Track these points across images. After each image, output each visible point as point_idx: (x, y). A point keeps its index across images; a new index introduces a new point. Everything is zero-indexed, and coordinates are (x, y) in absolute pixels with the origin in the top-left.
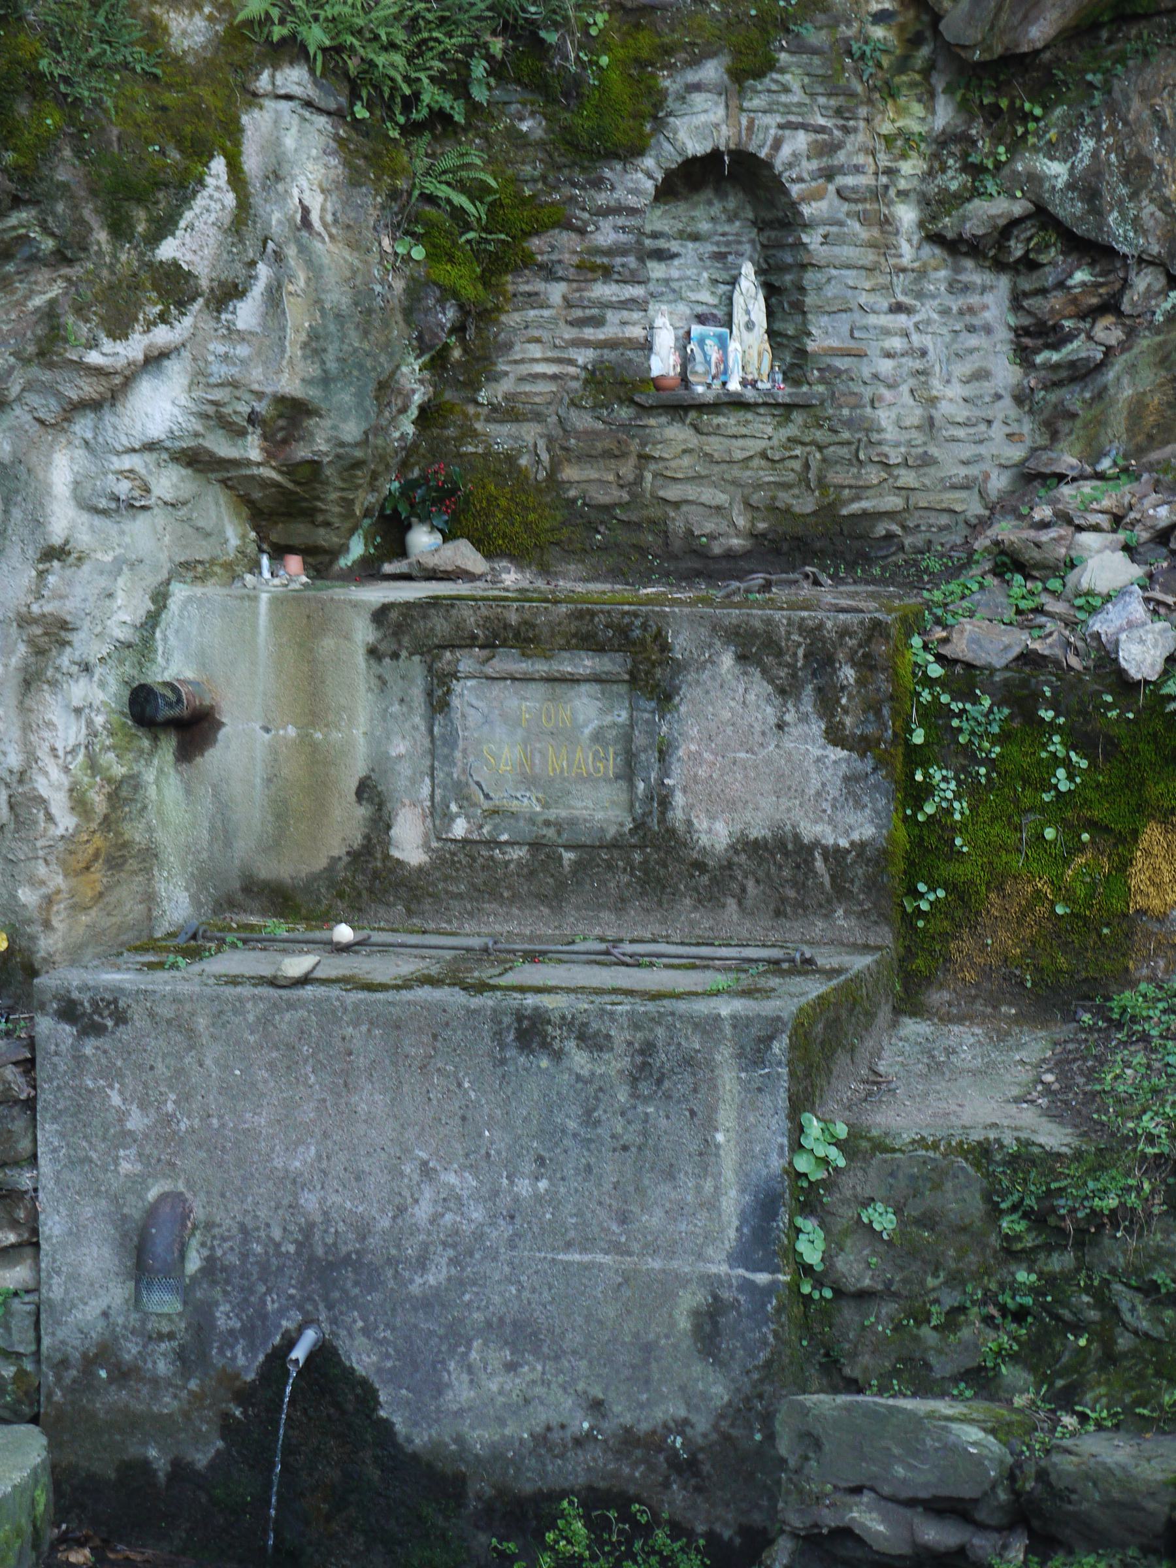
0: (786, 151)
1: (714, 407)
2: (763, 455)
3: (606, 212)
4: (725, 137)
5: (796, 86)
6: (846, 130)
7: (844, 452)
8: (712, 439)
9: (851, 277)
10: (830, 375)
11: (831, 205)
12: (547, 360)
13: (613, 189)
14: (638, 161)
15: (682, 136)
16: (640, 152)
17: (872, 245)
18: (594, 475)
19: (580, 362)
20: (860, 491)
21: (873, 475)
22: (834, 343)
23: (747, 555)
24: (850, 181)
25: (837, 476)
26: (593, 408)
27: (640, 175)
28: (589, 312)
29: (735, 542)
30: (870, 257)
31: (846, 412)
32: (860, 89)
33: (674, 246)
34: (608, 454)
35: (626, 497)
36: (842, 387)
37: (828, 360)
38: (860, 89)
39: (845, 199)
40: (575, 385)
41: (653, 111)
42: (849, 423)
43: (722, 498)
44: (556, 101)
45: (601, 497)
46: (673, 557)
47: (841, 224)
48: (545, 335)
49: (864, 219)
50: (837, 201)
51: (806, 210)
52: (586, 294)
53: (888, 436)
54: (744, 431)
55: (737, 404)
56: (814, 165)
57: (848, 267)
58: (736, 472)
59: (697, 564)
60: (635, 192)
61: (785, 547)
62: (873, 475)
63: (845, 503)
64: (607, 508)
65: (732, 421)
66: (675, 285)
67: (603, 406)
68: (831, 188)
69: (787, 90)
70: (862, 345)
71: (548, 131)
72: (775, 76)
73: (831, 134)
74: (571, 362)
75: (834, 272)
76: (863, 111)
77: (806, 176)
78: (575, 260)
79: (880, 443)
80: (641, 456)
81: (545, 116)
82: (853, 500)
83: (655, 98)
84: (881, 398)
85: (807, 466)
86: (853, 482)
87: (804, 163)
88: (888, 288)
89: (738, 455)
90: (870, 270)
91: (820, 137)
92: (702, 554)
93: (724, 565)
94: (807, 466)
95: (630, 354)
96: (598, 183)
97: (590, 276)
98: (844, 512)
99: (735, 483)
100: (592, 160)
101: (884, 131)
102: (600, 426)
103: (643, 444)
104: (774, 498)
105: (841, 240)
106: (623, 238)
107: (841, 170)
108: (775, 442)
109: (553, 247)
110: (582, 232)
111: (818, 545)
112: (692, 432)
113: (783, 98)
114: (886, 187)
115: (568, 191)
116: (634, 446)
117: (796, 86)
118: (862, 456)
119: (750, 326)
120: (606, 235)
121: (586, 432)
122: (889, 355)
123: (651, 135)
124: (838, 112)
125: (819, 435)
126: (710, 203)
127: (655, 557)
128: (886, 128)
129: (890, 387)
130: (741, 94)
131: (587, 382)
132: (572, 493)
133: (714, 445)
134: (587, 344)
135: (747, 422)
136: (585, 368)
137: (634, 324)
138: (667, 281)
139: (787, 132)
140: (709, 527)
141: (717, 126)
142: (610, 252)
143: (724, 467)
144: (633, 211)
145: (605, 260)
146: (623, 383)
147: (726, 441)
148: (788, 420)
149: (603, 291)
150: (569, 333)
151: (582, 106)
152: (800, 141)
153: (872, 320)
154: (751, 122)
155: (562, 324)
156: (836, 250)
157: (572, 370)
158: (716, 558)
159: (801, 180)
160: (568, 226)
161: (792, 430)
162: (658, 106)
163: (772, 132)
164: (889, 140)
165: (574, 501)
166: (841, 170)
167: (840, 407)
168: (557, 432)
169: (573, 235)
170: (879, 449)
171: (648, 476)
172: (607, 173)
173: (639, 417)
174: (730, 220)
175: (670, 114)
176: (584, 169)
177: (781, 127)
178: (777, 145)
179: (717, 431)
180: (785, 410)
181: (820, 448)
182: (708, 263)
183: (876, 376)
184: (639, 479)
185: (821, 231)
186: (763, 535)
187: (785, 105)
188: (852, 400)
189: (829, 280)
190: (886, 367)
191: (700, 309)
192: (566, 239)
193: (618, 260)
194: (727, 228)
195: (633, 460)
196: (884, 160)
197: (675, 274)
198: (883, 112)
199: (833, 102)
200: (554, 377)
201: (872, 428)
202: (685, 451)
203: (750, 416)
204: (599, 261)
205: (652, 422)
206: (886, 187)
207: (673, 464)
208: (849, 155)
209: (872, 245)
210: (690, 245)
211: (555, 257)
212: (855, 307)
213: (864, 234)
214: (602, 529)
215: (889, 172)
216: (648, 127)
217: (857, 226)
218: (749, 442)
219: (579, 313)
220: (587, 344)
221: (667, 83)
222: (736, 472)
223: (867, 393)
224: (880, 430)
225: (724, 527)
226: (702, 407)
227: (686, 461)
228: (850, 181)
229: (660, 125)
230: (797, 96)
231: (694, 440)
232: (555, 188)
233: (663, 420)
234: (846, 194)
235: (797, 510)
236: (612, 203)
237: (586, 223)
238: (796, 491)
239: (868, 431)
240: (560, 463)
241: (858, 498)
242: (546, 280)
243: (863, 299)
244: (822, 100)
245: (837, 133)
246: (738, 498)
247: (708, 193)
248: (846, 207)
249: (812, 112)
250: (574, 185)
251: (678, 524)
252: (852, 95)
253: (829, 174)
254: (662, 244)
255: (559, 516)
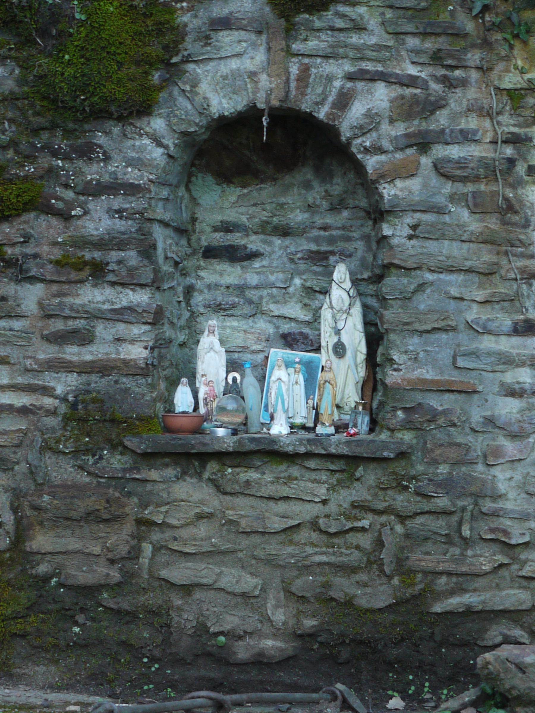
0: (357, 110)
1: (239, 457)
2: (314, 525)
3: (97, 190)
4: (265, 91)
5: (373, 23)
6: (449, 83)
7: (439, 525)
8: (239, 501)
9: (454, 284)
10: (420, 418)
11: (425, 185)
12: (14, 388)
13: (107, 158)
14: (142, 123)
15: (205, 88)
16: (145, 110)
17: (487, 240)
18: (74, 544)
19: (59, 390)
20: (464, 580)
21: (485, 559)
22: (428, 373)
23: (285, 662)
24: (455, 152)
25: (424, 559)
26: (76, 453)
27: (146, 141)
28: (72, 324)
29: (269, 643)
30: (485, 257)
31: (443, 469)
32: (470, 26)
33: (254, 243)
34: (92, 517)
35: (115, 575)
36: (440, 435)
37: (419, 397)
38: (470, 26)
39: (447, 177)
40: (52, 422)
41: (160, 52)
42: (447, 485)
43: (249, 582)
44: (30, 42)
45: (82, 575)
46: (178, 661)
47: (440, 211)
48: (14, 354)
49: (478, 206)
50: (435, 181)
51: (388, 191)
52: (69, 300)
53: (509, 505)
54: (285, 491)
55: (271, 453)
56: (400, 129)
57: (451, 270)
58: (273, 547)
59: (214, 673)
60: (137, 163)
61: (345, 654)
62: (485, 559)
63: (439, 596)
64: (90, 591)
65: (268, 477)
66: (251, 294)
67: (87, 452)
68: (425, 161)
69: (359, 28)
70: (470, 379)
71: (21, 81)
72: (342, 8)
73: (425, 86)
74: (47, 391)
75: (430, 277)
76: (474, 57)
77: (386, 144)
78: (57, 254)
79: (495, 514)
80: (141, 522)
81: (16, 59)
82: (452, 593)
83: (169, 37)
84: (497, 452)
85: (380, 543)
86: (451, 567)
87: (385, 127)
88: (513, 301)
89: (277, 524)
90: (488, 274)
91: (408, 91)
92: (220, 658)
93: (254, 674)
94: (380, 543)
95: (127, 382)
96: (87, 152)
97: (74, 276)
98: (438, 608)
99: (270, 562)
100: (76, 121)
101: (507, 84)
102: (84, 478)
103: (144, 505)
104: (327, 585)
105: (437, 233)
106: (120, 225)
107: (441, 137)
108: (332, 507)
109: (27, 239)
110: (65, 217)
111: (394, 652)
112: (211, 490)
113: (355, 39)
114: (511, 162)
115: (45, 161)
116: (132, 506)
117: (373, 23)
118: (466, 532)
119: (339, 350)
120: (98, 220)
121: (65, 486)
122: (512, 392)
123: (160, 89)
124: (437, 58)
125: (400, 501)
126: (307, 186)
127: (153, 660)
128: (511, 80)
129: (514, 436)
130: (290, 31)
131: (67, 419)
132: (43, 569)
133: (243, 509)
134: (66, 367)
135: (291, 478)
136: (64, 399)
137: (133, 342)
138: (241, 289)
139: (360, 85)
140: (231, 621)
141: (253, 75)
142: (101, 244)
143: (256, 539)
144: (133, 189)
145: (97, 255)
146: (113, 421)
147: (262, 505)
148: (353, 479)
149: (93, 296)
150: (45, 352)
151: (64, 50)
152: (381, 96)
153: (488, 343)
154: (305, 70)
155: (36, 340)
156: (432, 246)
157: (48, 402)
158: (242, 665)
159: (378, 150)
160: (48, 210)
161: (358, 492)
162: (172, 48)
163: (337, 84)
164: (515, 96)
165: (46, 579)
166: (441, 137)
167: (435, 462)
168: (27, 485)
169: (54, 221)
170: (495, 523)
171: (147, 549)
172: (100, 139)
173: (136, 468)
174: (333, 209)
175: (187, 60)
176: (68, 133)
177: (350, 77)
178: (344, 101)
179: (246, 490)
180: (349, 463)
181: (402, 519)
182: (302, 266)
183: (490, 421)
184: (135, 554)
185: (409, 219)
186: (312, 636)
187: (357, 48)
188: (453, 454)
189: (421, 287)
190: (509, 408)
191: (286, 327)
192: (44, 226)
193: (114, 255)
194: (329, 220)
195: (129, 527)
196: (508, 124)
197: (253, 279)
198: (507, 58)
199: (429, 45)
200: (24, 411)
201: (483, 492)
202: (200, 517)
203: (295, 471)
204: (88, 256)
205: (154, 475)
206: (511, 162)
207: (184, 533)
208: (454, 117)
209: (487, 240)
210: (278, 242)
211: (29, 250)
212: (462, 327)
213: (474, 224)
214: (81, 618)
215: (514, 140)
216: (156, 77)
217: (465, 214)
218: (295, 507)
219: (59, 325)
220: (66, 367)
221: (186, 18)
222: (273, 547)
223: (479, 444)
224: (497, 497)
225: (252, 622)
226: (222, 456)
227: (202, 529)
228: (455, 152)
229: (173, 72)
230: (375, 36)
231: (213, 502)
232: (30, 158)
233: (170, 472)
234: (449, 169)
235: (363, 602)
236: (106, 178)
237: (70, 205)
238: (363, 577)
239: (478, 496)
240: (30, 526)
241: (461, 590)
242: (18, 281)
243: (473, 314)
244: (412, 42)
245: (434, 86)
246: (276, 582)
247: (307, 173)
248: (448, 188)
249: (399, 59)
250: (55, 154)
251: (185, 617)
252: (458, 34)
253: (423, 143)
254: (236, 239)
255: (24, 597)
